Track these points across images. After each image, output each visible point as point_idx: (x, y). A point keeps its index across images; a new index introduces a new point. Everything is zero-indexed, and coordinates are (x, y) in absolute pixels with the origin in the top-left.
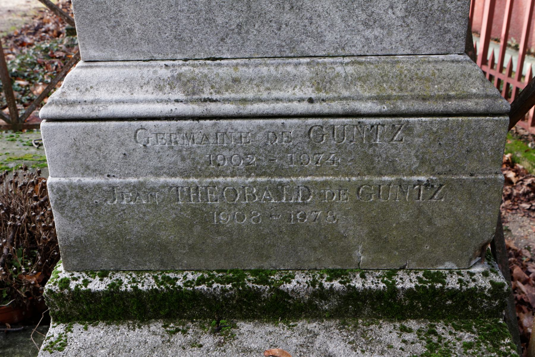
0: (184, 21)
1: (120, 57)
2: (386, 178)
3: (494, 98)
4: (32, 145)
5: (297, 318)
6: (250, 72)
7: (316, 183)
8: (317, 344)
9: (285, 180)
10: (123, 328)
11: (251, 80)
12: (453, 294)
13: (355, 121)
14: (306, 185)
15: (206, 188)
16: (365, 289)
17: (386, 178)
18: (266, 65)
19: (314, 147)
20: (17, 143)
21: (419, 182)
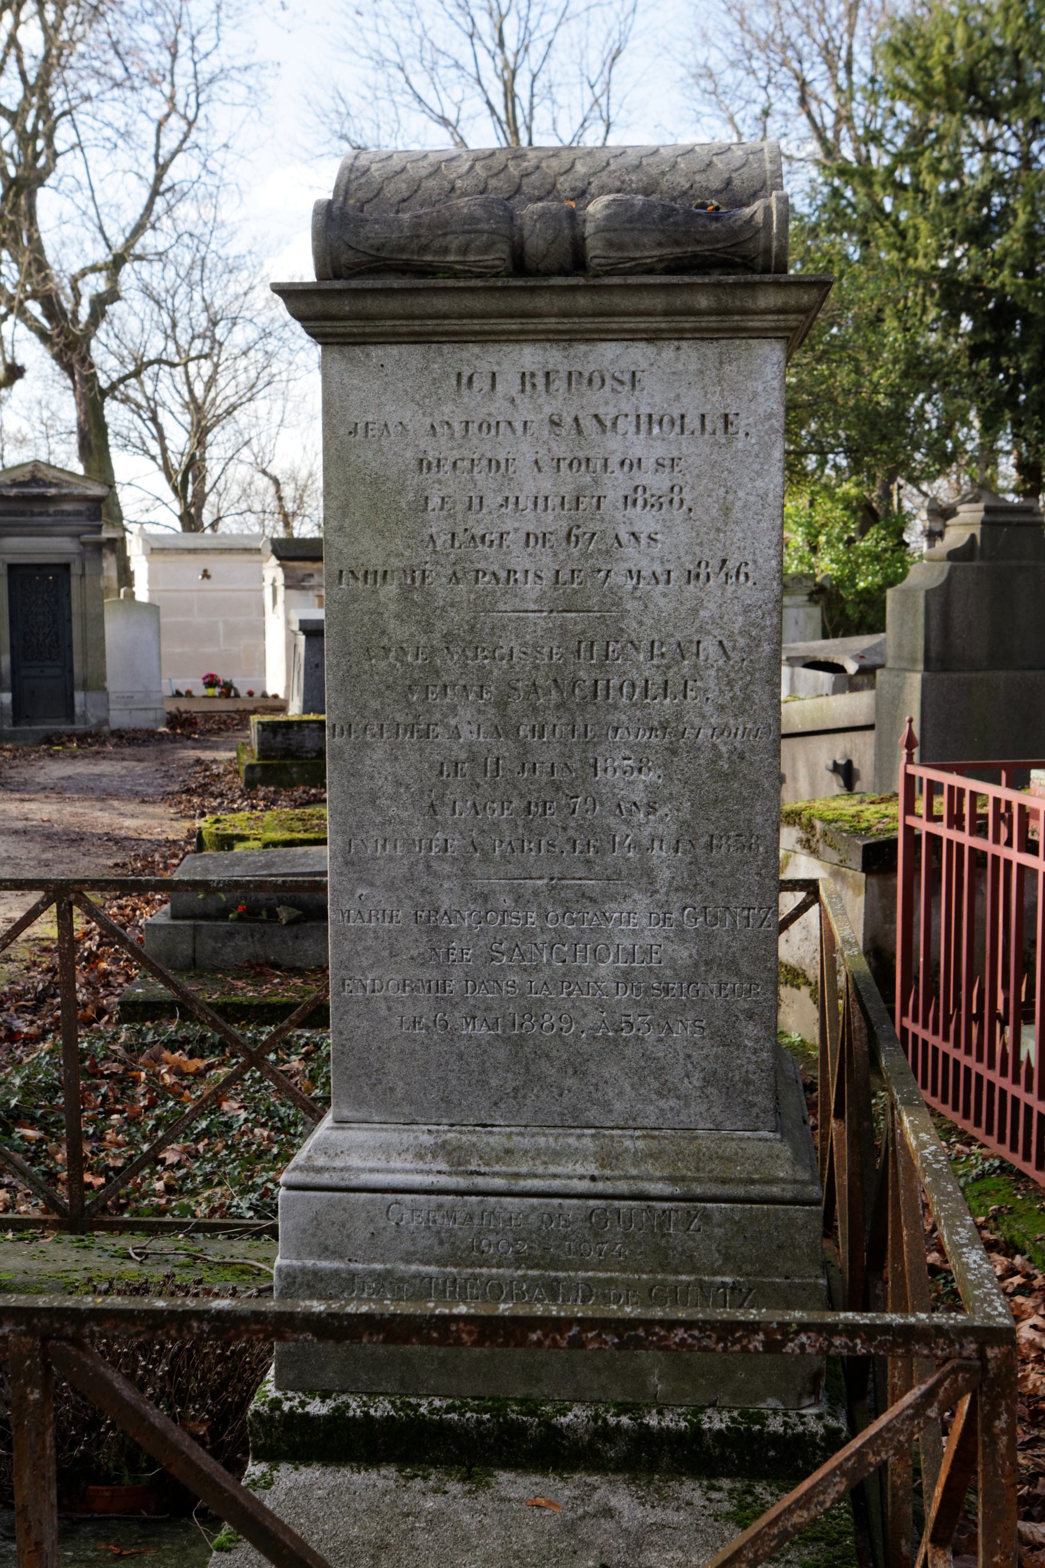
0: (454, 1082)
1: (376, 1119)
2: (684, 1277)
3: (805, 1183)
4: (130, 1257)
5: (574, 1469)
6: (525, 1142)
7: (599, 1280)
8: (596, 1497)
9: (561, 1274)
10: (345, 1471)
11: (526, 1152)
12: (775, 1439)
13: (643, 1204)
14: (587, 1282)
15: (466, 1280)
16: (662, 1429)
17: (684, 1277)
18: (545, 1135)
19: (596, 1235)
20: (96, 1252)
21: (724, 1284)
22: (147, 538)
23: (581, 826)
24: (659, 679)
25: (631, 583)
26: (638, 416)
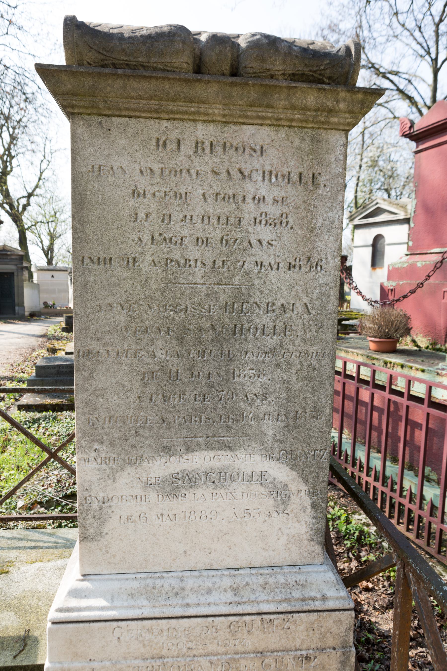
22: (36, 267)
23: (225, 407)
24: (271, 324)
25: (257, 269)
26: (264, 172)
